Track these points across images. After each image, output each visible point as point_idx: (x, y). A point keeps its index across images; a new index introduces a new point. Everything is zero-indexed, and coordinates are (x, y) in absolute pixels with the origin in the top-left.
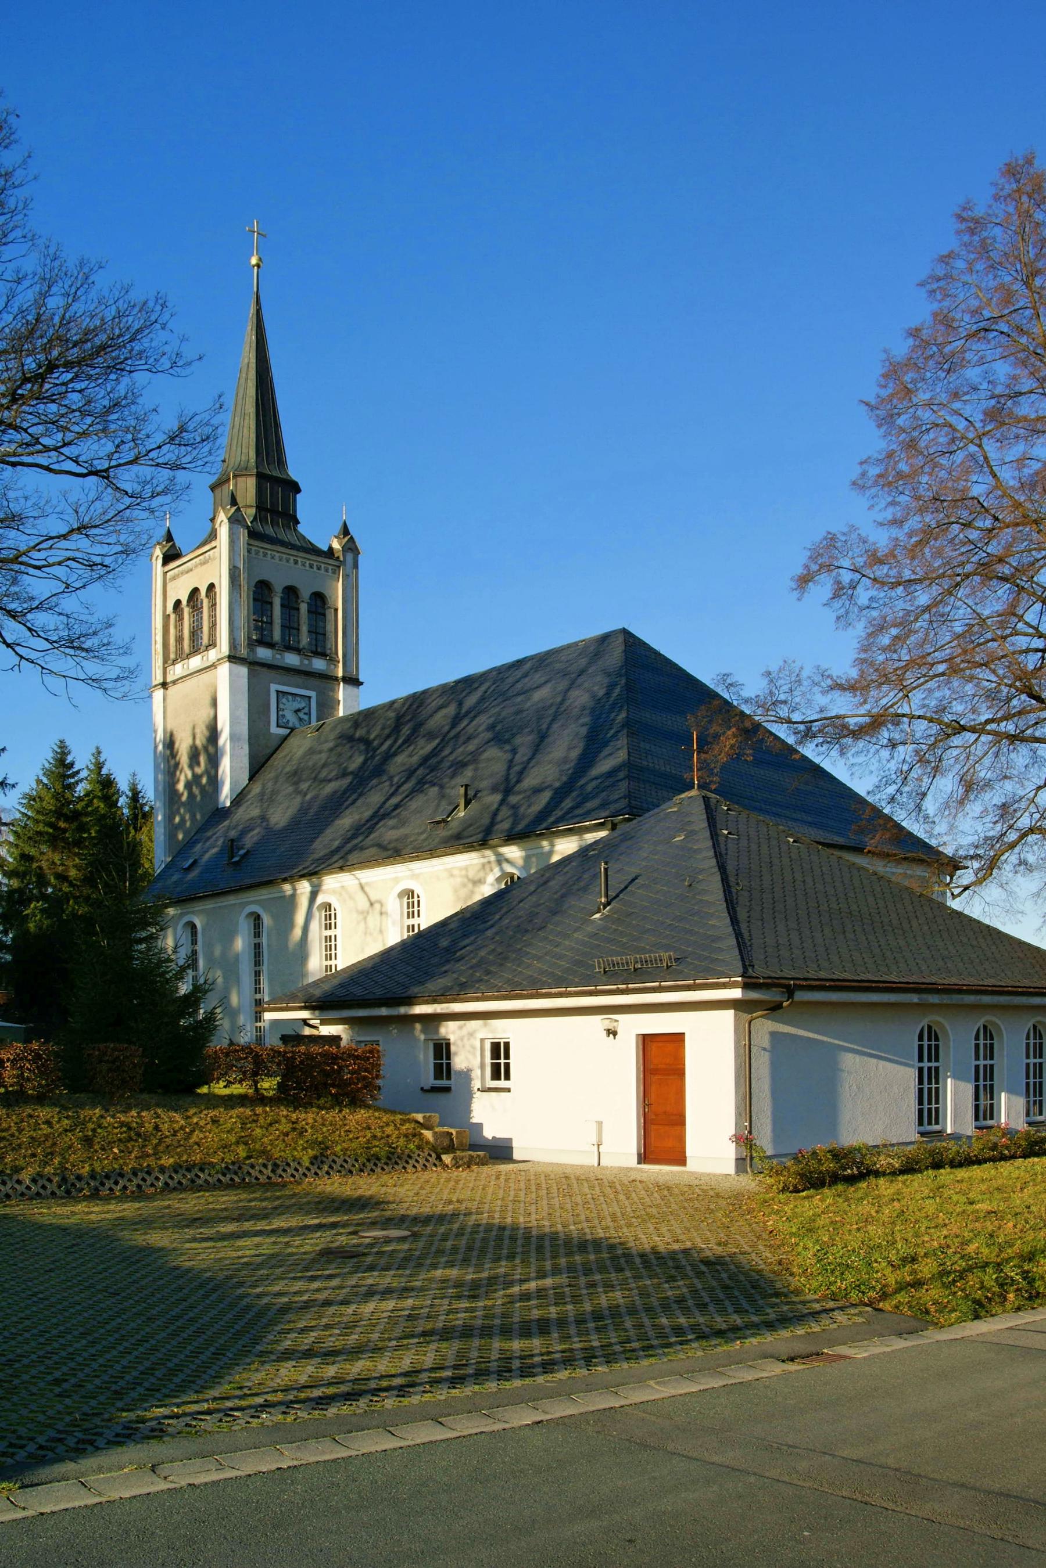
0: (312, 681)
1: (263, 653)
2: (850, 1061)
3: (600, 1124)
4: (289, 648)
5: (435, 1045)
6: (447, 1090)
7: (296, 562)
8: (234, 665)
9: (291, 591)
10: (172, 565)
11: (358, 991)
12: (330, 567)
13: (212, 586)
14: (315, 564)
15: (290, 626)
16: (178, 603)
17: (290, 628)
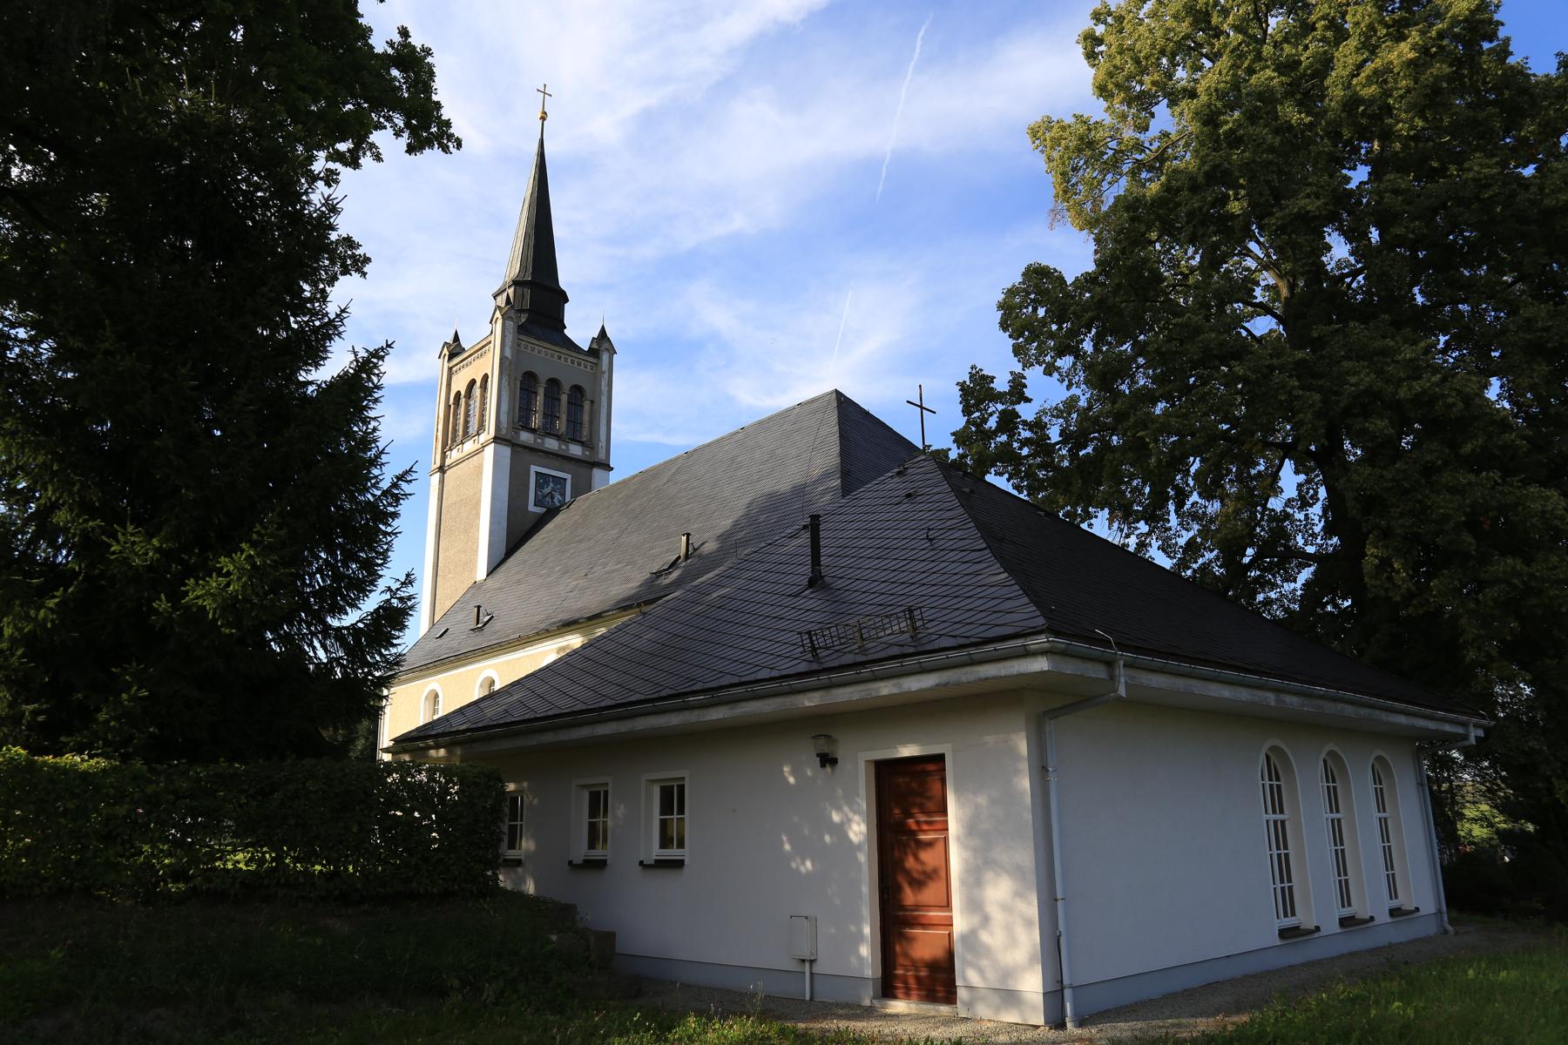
1: (525, 437)
4: (575, 440)
5: (663, 789)
6: (678, 864)
9: (554, 384)
10: (456, 360)
13: (486, 377)
16: (458, 393)
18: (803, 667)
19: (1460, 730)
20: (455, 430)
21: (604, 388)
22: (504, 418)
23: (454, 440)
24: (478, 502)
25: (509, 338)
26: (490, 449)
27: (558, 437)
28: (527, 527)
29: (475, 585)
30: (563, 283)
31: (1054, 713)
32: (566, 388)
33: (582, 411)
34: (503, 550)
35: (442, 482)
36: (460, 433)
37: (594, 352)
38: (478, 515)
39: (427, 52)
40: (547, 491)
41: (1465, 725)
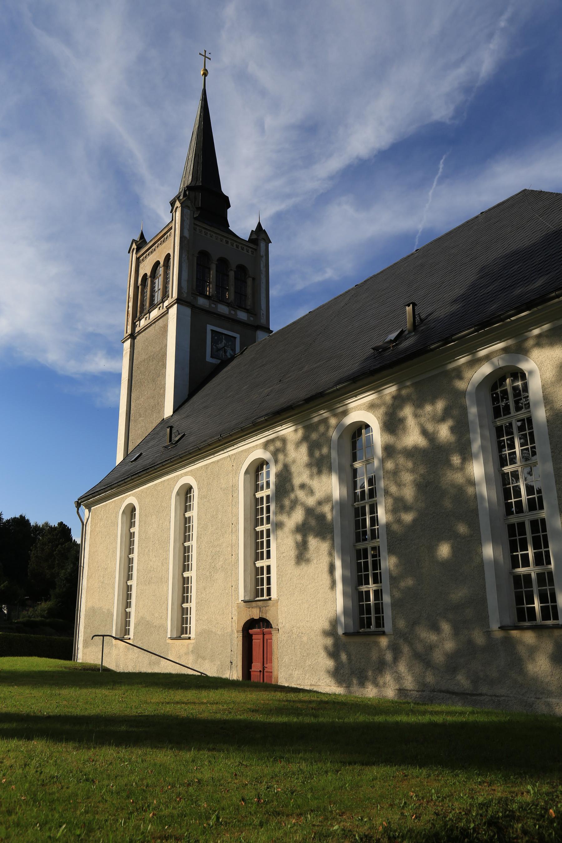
1: (202, 301)
2: (241, 679)
4: (221, 300)
7: (227, 242)
8: (181, 306)
9: (223, 263)
12: (250, 250)
14: (240, 246)
16: (145, 275)
20: (142, 305)
22: (184, 284)
23: (141, 312)
24: (164, 355)
25: (187, 222)
26: (173, 311)
27: (229, 305)
30: (225, 189)
34: (186, 392)
35: (132, 346)
36: (148, 305)
38: (164, 366)
40: (220, 346)
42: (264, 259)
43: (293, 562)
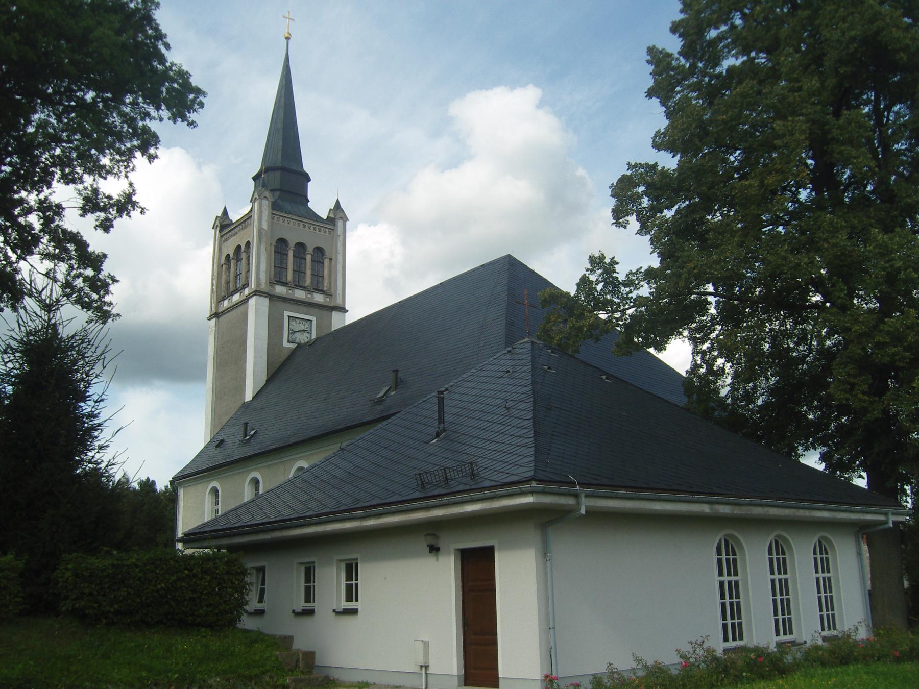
0: (312, 310)
1: (280, 290)
3: (426, 644)
4: (299, 286)
6: (354, 612)
9: (301, 246)
11: (246, 519)
13: (248, 243)
15: (299, 271)
16: (228, 256)
17: (300, 272)
18: (417, 495)
19: (882, 518)
21: (340, 248)
28: (282, 359)
29: (246, 406)
30: (307, 167)
31: (551, 522)
32: (310, 249)
33: (323, 267)
37: (331, 221)
39: (148, 479)
41: (886, 514)
42: (341, 238)
43: (603, 252)
